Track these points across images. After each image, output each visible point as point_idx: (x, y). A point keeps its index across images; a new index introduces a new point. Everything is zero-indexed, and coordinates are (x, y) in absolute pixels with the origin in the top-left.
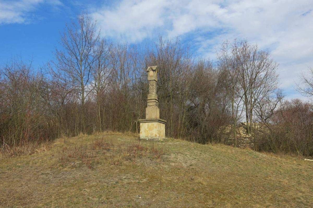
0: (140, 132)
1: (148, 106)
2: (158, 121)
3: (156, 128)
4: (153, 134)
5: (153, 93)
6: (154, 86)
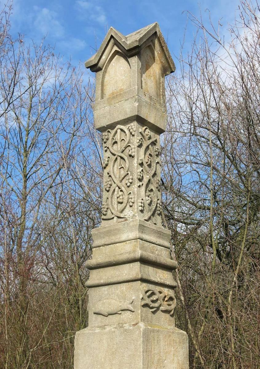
1: (93, 319)
5: (128, 212)
6: (135, 162)
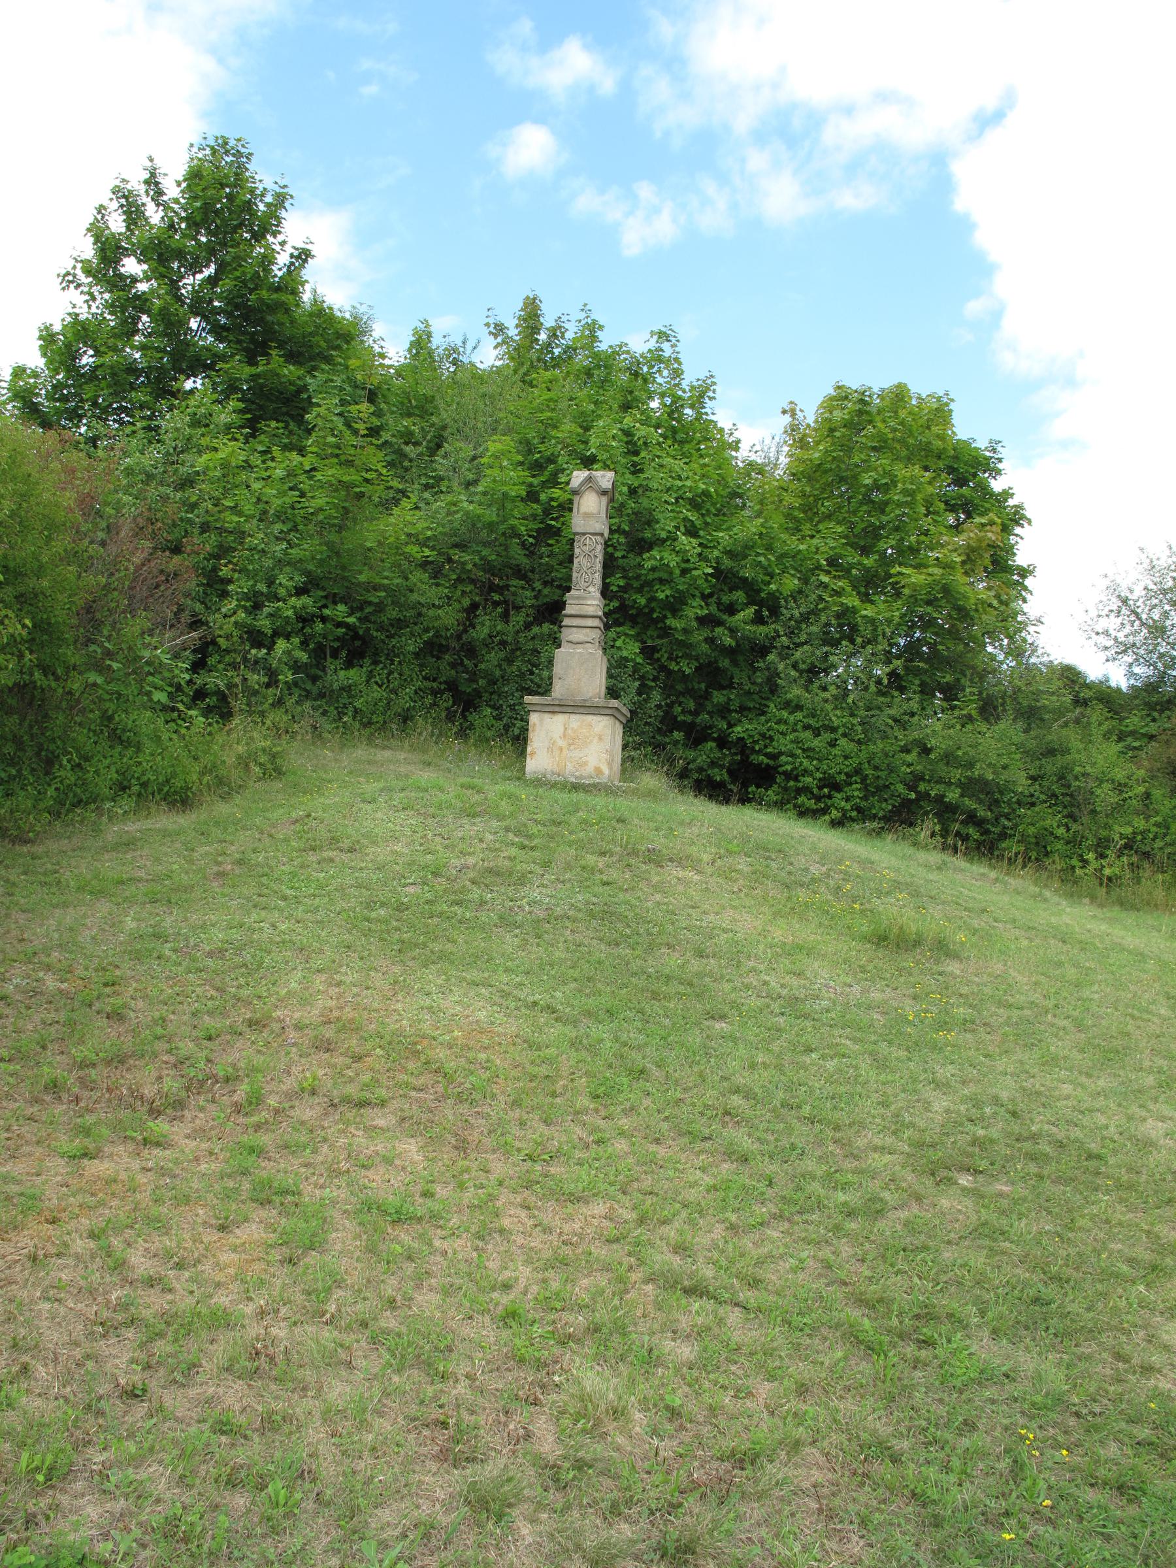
0: (529, 749)
2: (610, 711)
3: (600, 739)
4: (586, 764)
